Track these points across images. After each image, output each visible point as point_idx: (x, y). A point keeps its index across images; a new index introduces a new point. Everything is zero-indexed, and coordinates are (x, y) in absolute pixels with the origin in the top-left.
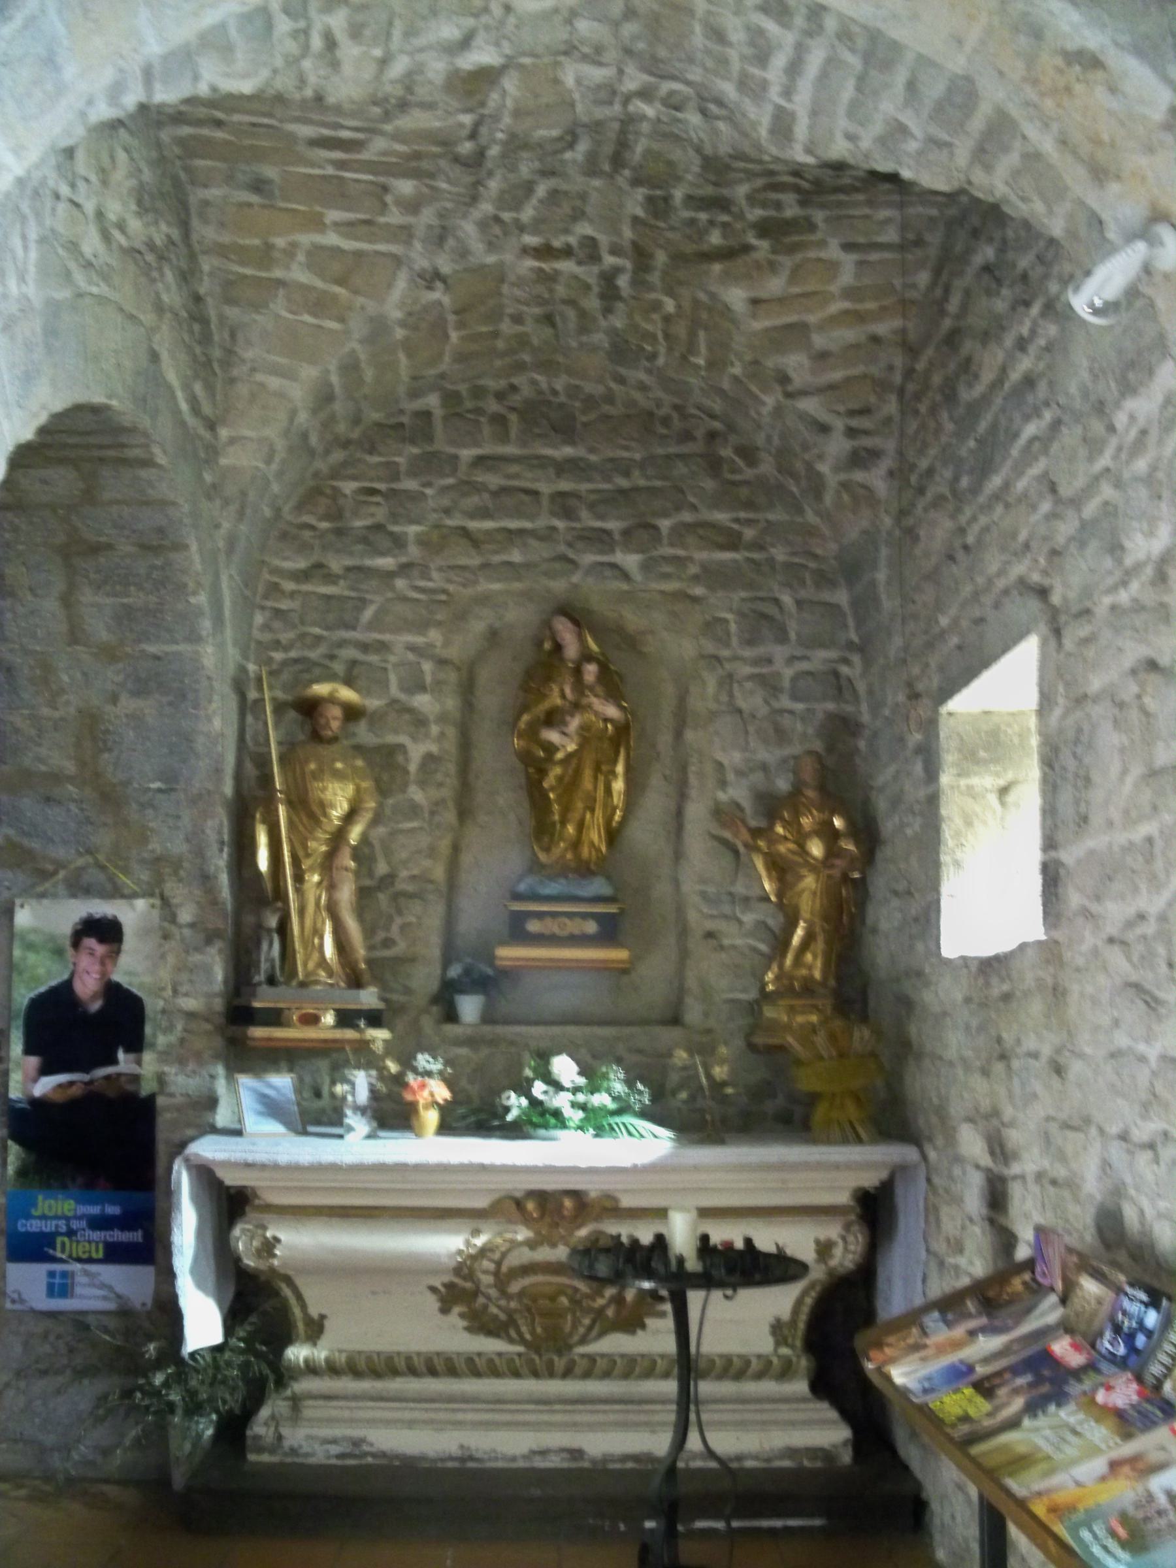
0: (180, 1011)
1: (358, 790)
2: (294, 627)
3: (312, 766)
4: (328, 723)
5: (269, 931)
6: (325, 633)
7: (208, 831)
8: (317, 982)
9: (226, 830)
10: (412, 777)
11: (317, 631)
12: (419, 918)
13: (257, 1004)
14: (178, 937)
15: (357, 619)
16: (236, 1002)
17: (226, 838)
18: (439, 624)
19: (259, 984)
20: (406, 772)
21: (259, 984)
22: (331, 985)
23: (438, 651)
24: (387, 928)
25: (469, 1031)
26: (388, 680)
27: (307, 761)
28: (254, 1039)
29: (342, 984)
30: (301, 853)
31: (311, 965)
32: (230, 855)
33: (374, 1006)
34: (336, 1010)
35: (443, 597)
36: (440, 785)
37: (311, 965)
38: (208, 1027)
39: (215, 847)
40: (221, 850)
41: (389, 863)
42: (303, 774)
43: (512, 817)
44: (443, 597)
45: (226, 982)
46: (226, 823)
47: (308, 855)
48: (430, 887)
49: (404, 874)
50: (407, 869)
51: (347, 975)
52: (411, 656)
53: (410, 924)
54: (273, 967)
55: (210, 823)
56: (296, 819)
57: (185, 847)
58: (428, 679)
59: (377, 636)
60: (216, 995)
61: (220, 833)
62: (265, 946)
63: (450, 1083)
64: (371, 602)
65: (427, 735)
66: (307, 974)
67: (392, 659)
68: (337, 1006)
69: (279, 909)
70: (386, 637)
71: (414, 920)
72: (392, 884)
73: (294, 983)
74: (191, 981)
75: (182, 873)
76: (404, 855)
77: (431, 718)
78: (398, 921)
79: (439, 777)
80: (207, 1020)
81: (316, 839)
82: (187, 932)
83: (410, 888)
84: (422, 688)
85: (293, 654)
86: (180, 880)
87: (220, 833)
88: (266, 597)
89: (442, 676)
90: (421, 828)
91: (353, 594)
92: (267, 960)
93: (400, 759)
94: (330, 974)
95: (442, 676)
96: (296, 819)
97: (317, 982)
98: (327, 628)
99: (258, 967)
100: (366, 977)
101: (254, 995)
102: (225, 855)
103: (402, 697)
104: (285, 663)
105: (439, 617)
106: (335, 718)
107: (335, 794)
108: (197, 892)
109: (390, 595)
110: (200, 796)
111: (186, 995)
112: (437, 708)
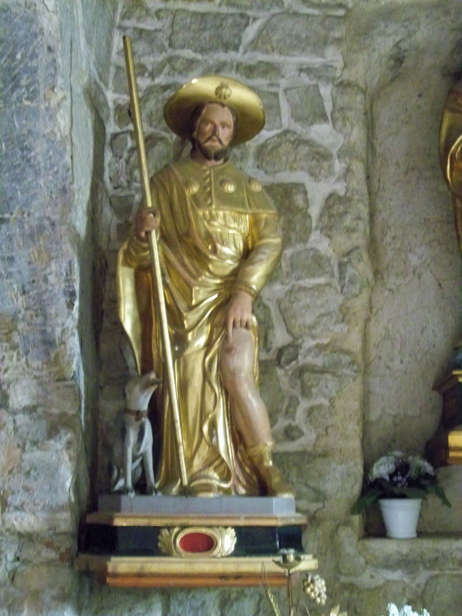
0: (11, 531)
1: (255, 222)
2: (162, 49)
3: (195, 189)
4: (214, 131)
5: (138, 414)
6: (199, 57)
7: (52, 279)
8: (208, 488)
9: (76, 276)
10: (314, 224)
11: (188, 53)
12: (331, 400)
13: (119, 522)
14: (10, 427)
15: (238, 36)
16: (91, 519)
17: (77, 287)
18: (338, 41)
19: (124, 491)
20: (307, 216)
21: (124, 491)
22: (227, 492)
23: (338, 74)
24: (289, 414)
25: (405, 549)
26: (279, 108)
27: (187, 184)
28: (115, 575)
29: (242, 491)
30: (182, 305)
31: (197, 463)
32: (81, 313)
33: (293, 521)
34: (239, 530)
35: (341, 12)
36: (350, 231)
37: (197, 463)
38: (52, 555)
39: (63, 301)
40: (70, 305)
41: (289, 331)
42: (182, 198)
43: (428, 278)
44: (341, 12)
45: (76, 487)
46: (76, 266)
47: (191, 308)
48: (346, 359)
49: (309, 343)
50: (314, 337)
51: (248, 478)
52: (305, 79)
53: (320, 407)
54: (143, 464)
55: (54, 266)
56: (172, 258)
57: (21, 301)
58: (328, 107)
59: (261, 57)
60: (62, 508)
61: (68, 280)
62: (132, 436)
63: (343, 593)
64: (255, 19)
65: (331, 172)
66: (192, 479)
67: (284, 83)
68: (241, 522)
69: (152, 383)
70: (275, 58)
71: (326, 402)
72: (295, 357)
73: (175, 490)
74: (27, 489)
75: (16, 338)
76: (309, 320)
77: (334, 152)
78: (304, 404)
79: (348, 221)
80: (49, 545)
81: (203, 285)
82: (22, 419)
83: (319, 361)
84: (323, 117)
85: (161, 80)
86: (14, 347)
87: (68, 280)
88: (125, 16)
89: (343, 101)
90: (328, 285)
91: (232, 10)
92: (134, 458)
93: (299, 200)
94: (226, 477)
95: (343, 101)
96: (172, 258)
97: (208, 488)
98: (202, 51)
99: (123, 465)
100: (276, 480)
101: (117, 508)
102: (75, 312)
103: (297, 127)
104: (150, 90)
105: (337, 34)
106: (224, 125)
107: (226, 226)
108: (36, 364)
109: (276, 10)
110: (41, 228)
111: (20, 508)
112: (341, 140)
